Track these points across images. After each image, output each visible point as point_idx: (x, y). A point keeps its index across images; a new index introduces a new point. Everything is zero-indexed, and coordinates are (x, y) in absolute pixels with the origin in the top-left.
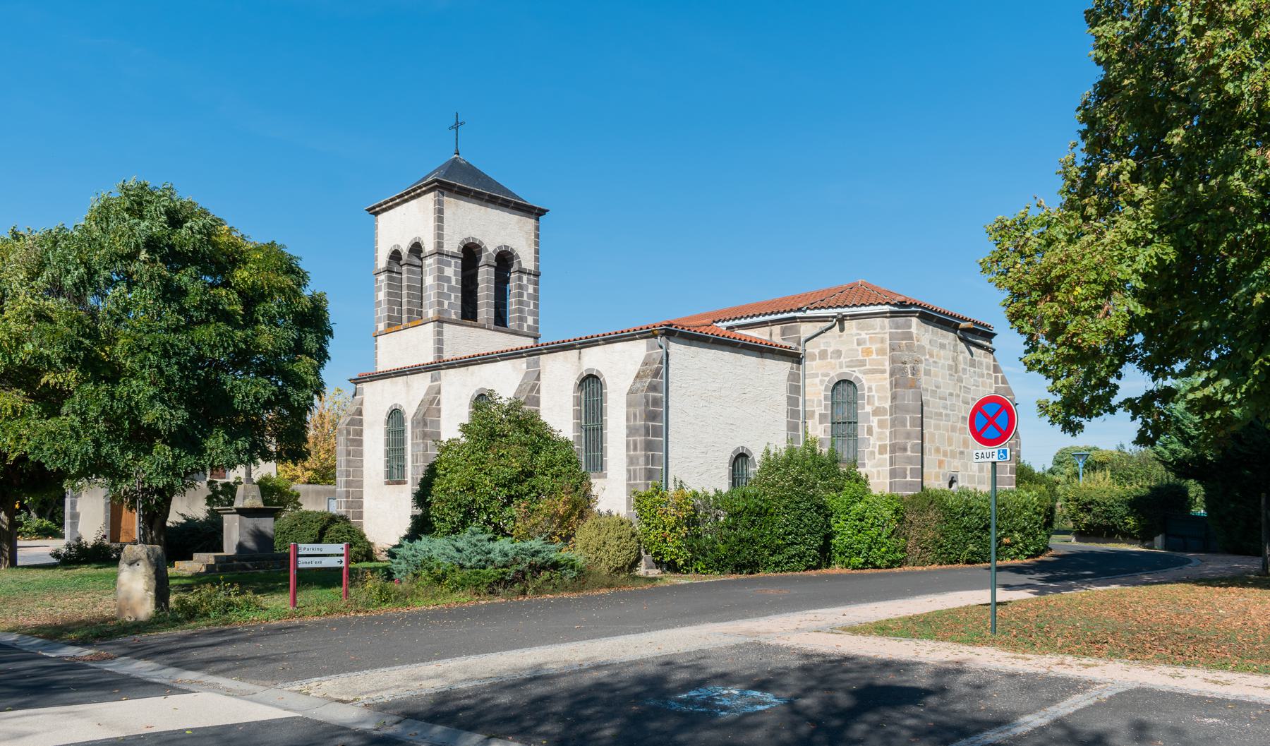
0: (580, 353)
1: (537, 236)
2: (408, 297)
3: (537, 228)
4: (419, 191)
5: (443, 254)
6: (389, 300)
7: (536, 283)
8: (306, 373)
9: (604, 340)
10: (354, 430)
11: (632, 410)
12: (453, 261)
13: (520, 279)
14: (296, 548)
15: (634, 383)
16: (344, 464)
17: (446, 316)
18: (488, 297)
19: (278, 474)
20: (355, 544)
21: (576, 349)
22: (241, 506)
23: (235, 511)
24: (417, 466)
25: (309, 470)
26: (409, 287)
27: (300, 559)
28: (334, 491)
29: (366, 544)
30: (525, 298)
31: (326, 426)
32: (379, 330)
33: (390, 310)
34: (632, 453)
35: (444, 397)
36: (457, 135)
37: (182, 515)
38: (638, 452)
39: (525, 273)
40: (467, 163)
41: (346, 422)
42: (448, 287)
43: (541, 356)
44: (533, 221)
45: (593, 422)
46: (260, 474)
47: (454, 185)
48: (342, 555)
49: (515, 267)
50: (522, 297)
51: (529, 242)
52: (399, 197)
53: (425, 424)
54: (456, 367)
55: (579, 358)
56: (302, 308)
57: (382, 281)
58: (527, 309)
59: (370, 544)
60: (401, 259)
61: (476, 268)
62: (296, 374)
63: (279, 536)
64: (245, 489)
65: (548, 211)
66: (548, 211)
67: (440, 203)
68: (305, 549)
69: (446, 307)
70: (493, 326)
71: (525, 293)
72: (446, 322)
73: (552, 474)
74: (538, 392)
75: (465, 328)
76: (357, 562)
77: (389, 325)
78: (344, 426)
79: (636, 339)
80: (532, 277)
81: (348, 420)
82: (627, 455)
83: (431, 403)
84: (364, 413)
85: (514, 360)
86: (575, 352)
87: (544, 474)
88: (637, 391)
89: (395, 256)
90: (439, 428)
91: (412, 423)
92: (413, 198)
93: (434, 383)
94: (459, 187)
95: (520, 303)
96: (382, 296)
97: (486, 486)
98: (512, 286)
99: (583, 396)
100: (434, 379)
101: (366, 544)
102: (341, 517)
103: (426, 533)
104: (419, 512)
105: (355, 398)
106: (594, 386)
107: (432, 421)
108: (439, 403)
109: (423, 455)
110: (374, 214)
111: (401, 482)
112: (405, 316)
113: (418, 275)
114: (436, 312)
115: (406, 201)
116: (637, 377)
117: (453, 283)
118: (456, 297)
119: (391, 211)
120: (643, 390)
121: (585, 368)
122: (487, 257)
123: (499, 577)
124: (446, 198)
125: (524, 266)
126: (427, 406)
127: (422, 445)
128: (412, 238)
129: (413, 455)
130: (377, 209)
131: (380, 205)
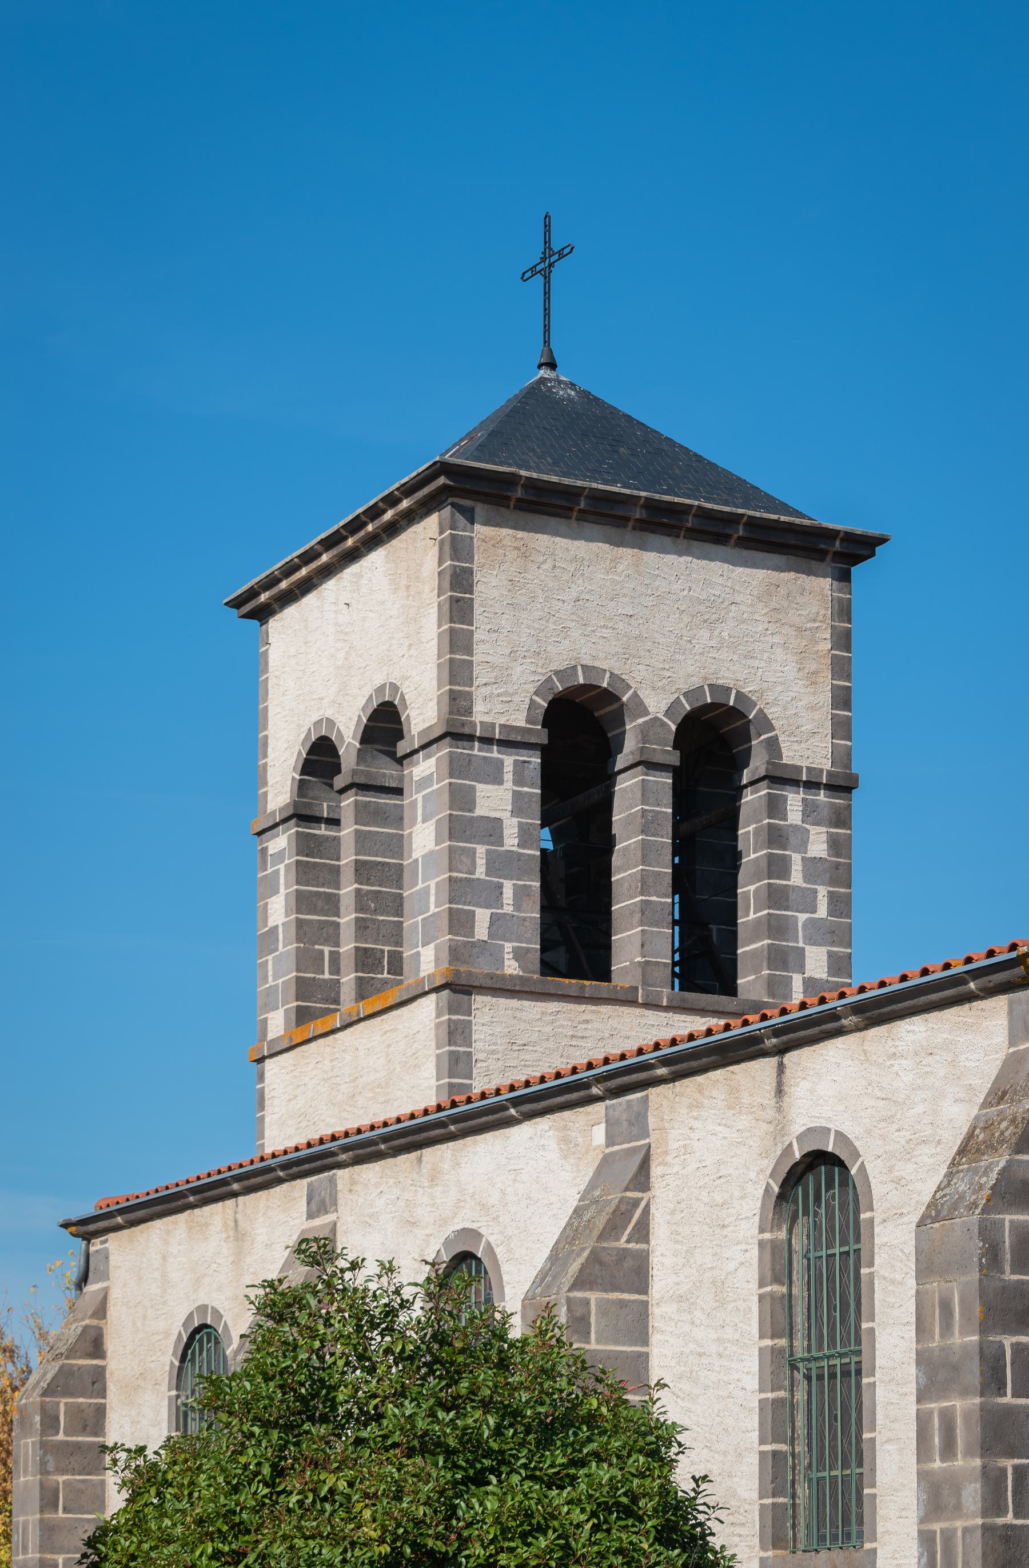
0: (781, 1068)
1: (843, 640)
2: (360, 907)
3: (844, 611)
4: (389, 515)
5: (470, 738)
6: (300, 924)
7: (841, 819)
9: (857, 1009)
10: (74, 1412)
11: (934, 1286)
12: (509, 761)
13: (775, 807)
15: (950, 1175)
16: (33, 1538)
17: (481, 968)
18: (645, 884)
21: (764, 1054)
30: (796, 878)
32: (271, 1035)
33: (306, 959)
34: (937, 1464)
36: (547, 293)
38: (959, 1462)
39: (795, 783)
40: (585, 394)
41: (44, 1384)
42: (490, 857)
43: (653, 1092)
44: (825, 584)
45: (820, 1347)
47: (510, 480)
49: (757, 765)
50: (785, 874)
51: (813, 666)
52: (328, 543)
54: (379, 1156)
55: (780, 1091)
57: (280, 856)
58: (802, 917)
60: (337, 769)
65: (882, 540)
66: (882, 540)
69: (481, 932)
70: (665, 995)
71: (796, 859)
72: (483, 990)
74: (642, 1232)
75: (553, 1006)
77: (302, 1016)
78: (35, 1398)
79: (970, 998)
80: (822, 796)
81: (49, 1377)
82: (922, 1475)
84: (111, 1345)
85: (566, 1114)
86: (763, 1068)
88: (955, 1207)
92: (373, 542)
93: (317, 1222)
95: (777, 897)
100: (318, 1206)
112: (348, 979)
114: (445, 955)
115: (352, 556)
116: (962, 1151)
117: (511, 841)
118: (520, 893)
119: (310, 600)
120: (974, 1205)
121: (797, 1129)
122: (644, 733)
124: (481, 531)
125: (793, 754)
128: (368, 690)
130: (263, 597)
131: (271, 582)
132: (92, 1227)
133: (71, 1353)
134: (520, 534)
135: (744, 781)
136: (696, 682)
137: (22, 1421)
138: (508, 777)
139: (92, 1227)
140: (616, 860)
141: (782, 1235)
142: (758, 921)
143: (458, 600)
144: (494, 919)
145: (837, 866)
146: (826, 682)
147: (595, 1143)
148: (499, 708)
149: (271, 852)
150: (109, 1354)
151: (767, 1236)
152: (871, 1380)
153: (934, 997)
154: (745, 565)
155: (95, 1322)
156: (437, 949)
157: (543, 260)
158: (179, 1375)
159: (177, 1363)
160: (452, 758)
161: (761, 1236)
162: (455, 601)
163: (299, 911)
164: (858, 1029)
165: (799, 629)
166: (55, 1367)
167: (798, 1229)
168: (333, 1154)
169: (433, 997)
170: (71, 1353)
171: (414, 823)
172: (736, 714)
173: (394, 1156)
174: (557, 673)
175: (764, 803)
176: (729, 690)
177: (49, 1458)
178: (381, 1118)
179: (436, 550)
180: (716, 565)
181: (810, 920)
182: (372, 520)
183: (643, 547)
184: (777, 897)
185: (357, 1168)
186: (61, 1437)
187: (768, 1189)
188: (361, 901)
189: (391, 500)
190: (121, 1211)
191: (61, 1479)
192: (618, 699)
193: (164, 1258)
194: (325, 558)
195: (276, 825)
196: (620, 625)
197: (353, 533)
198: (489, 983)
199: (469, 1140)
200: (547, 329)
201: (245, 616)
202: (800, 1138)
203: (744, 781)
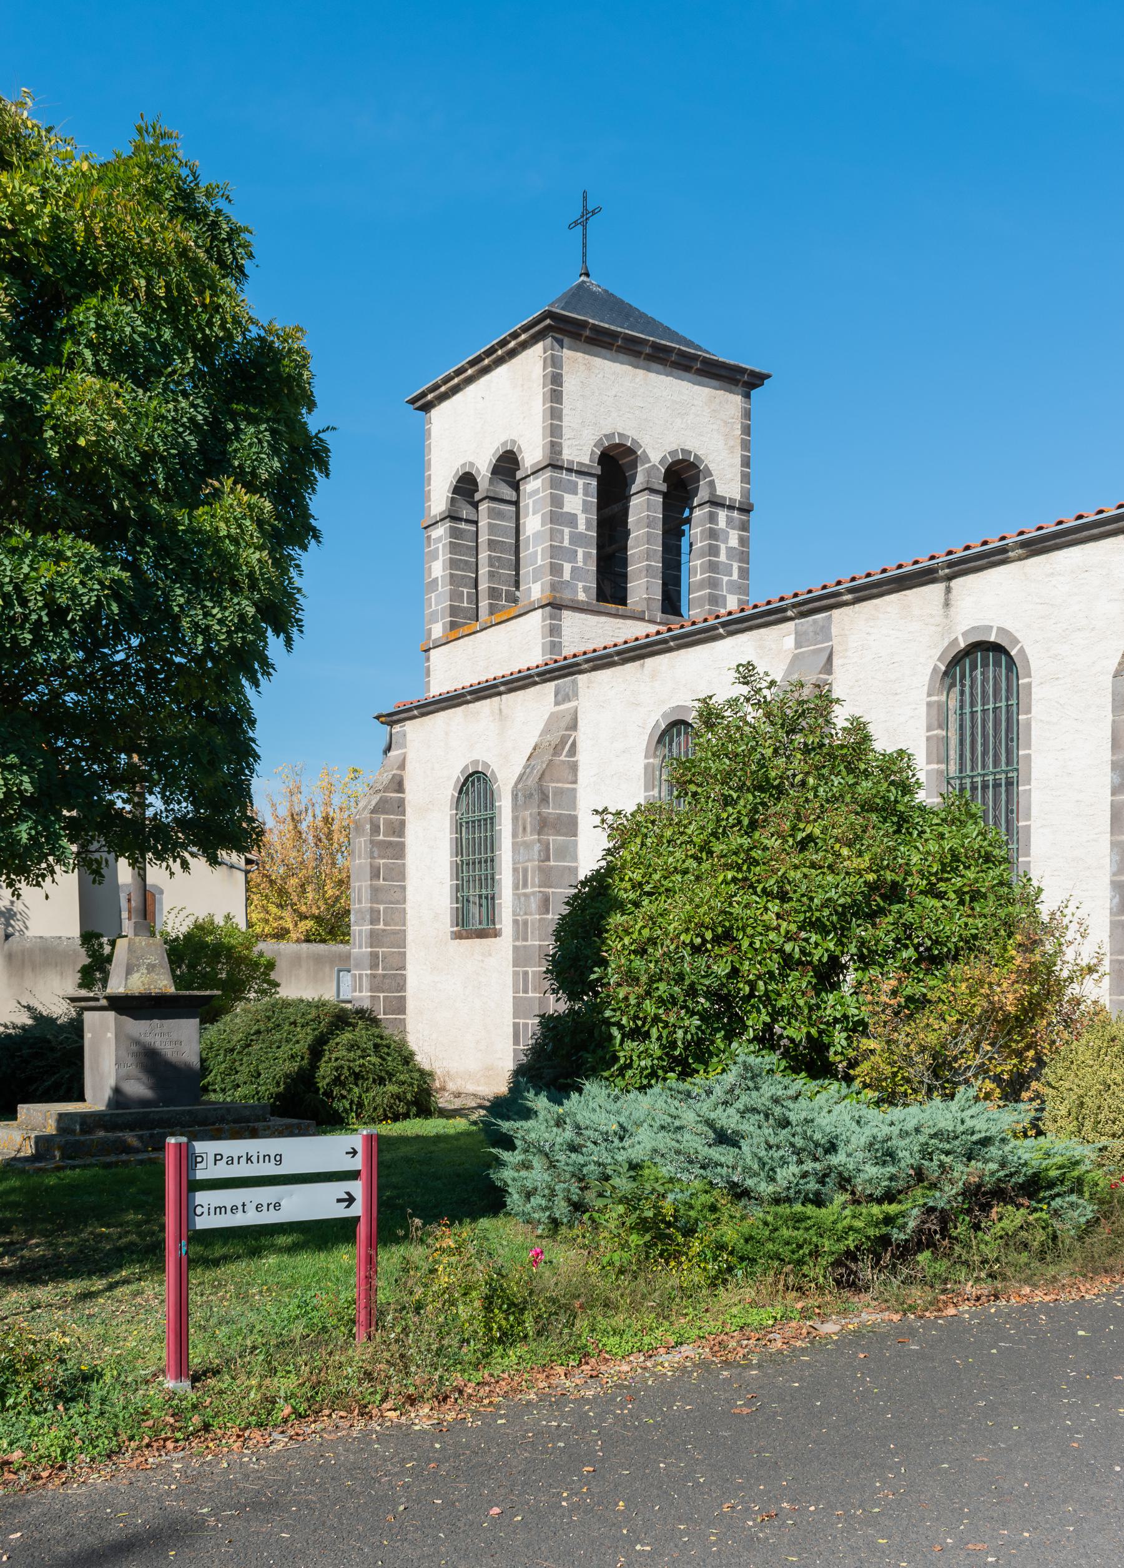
0: (948, 590)
1: (746, 430)
2: (491, 565)
3: (747, 414)
4: (512, 344)
5: (561, 468)
6: (452, 575)
7: (744, 527)
8: (235, 541)
9: (1024, 545)
12: (581, 482)
13: (713, 518)
14: (189, 1160)
16: (366, 894)
17: (566, 596)
18: (649, 555)
19: (250, 925)
20: (391, 1075)
21: (933, 581)
22: (121, 990)
23: (104, 1002)
24: (526, 895)
25: (306, 918)
26: (492, 544)
27: (201, 1197)
28: (348, 956)
29: (416, 1075)
30: (723, 557)
31: (335, 837)
32: (433, 637)
33: (455, 595)
35: (584, 736)
36: (585, 236)
37: (29, 1008)
39: (722, 505)
40: (606, 291)
42: (571, 534)
43: (836, 613)
45: (996, 763)
46: (192, 919)
47: (583, 324)
48: (353, 1175)
49: (703, 494)
50: (717, 555)
51: (731, 443)
52: (472, 363)
53: (544, 799)
55: (947, 604)
56: (223, 327)
57: (439, 539)
58: (726, 579)
59: (423, 1073)
61: (626, 498)
62: (211, 540)
63: (221, 1058)
64: (131, 949)
65: (768, 376)
66: (768, 376)
67: (555, 362)
68: (218, 1158)
69: (567, 576)
70: (659, 616)
71: (723, 547)
72: (568, 608)
73: (959, 893)
75: (603, 619)
76: (396, 1118)
77: (453, 625)
78: (366, 814)
80: (735, 514)
81: (373, 803)
83: (557, 750)
84: (407, 785)
85: (762, 631)
87: (932, 891)
89: (465, 485)
90: (575, 809)
91: (515, 797)
92: (500, 361)
94: (595, 328)
95: (713, 567)
96: (438, 569)
97: (768, 928)
98: (696, 533)
99: (954, 704)
100: (561, 698)
101: (416, 1075)
102: (361, 1013)
103: (593, 1072)
104: (558, 1005)
105: (391, 754)
106: (984, 674)
107: (559, 792)
108: (573, 751)
109: (540, 869)
110: (420, 409)
111: (488, 931)
113: (509, 520)
115: (486, 370)
118: (587, 555)
119: (458, 397)
122: (649, 472)
123: (872, 1232)
124: (566, 353)
126: (547, 757)
127: (537, 847)
129: (515, 870)
130: (430, 397)
131: (436, 387)
132: (395, 718)
133: (386, 790)
134: (587, 357)
135: (695, 504)
136: (674, 447)
137: (357, 828)
138: (580, 491)
139: (395, 718)
140: (630, 543)
141: (944, 698)
142: (703, 579)
143: (555, 391)
144: (573, 569)
145: (743, 552)
146: (738, 453)
147: (785, 648)
148: (576, 453)
149: (433, 537)
150: (407, 791)
151: (934, 698)
152: (1027, 787)
153: (1095, 531)
154: (699, 384)
155: (399, 772)
156: (542, 584)
157: (582, 216)
158: (458, 801)
159: (456, 795)
160: (552, 478)
161: (929, 699)
162: (553, 391)
163: (451, 569)
164: (1020, 559)
165: (726, 423)
166: (377, 797)
167: (951, 695)
168: (578, 664)
169: (540, 611)
170: (386, 790)
171: (527, 515)
172: (693, 466)
173: (622, 664)
174: (605, 436)
175: (707, 516)
176: (690, 452)
177: (375, 849)
178: (583, 649)
179: (542, 363)
180: (685, 383)
181: (729, 581)
182: (501, 348)
183: (648, 370)
184: (713, 567)
185: (594, 673)
186: (381, 837)
187: (935, 669)
188: (491, 561)
189: (515, 335)
190: (417, 707)
191: (382, 861)
192: (635, 453)
193: (447, 734)
194: (470, 372)
195: (437, 522)
196: (637, 412)
197: (488, 356)
198: (570, 604)
199: (683, 651)
200: (584, 255)
201: (417, 409)
202: (964, 634)
203: (695, 504)
